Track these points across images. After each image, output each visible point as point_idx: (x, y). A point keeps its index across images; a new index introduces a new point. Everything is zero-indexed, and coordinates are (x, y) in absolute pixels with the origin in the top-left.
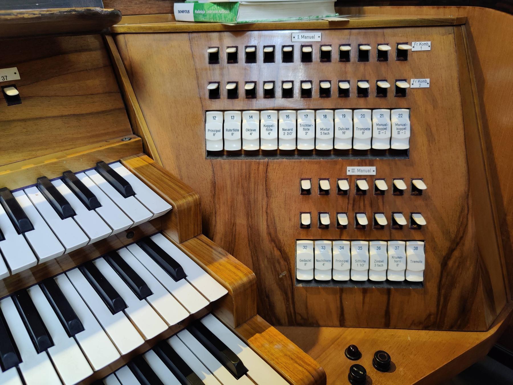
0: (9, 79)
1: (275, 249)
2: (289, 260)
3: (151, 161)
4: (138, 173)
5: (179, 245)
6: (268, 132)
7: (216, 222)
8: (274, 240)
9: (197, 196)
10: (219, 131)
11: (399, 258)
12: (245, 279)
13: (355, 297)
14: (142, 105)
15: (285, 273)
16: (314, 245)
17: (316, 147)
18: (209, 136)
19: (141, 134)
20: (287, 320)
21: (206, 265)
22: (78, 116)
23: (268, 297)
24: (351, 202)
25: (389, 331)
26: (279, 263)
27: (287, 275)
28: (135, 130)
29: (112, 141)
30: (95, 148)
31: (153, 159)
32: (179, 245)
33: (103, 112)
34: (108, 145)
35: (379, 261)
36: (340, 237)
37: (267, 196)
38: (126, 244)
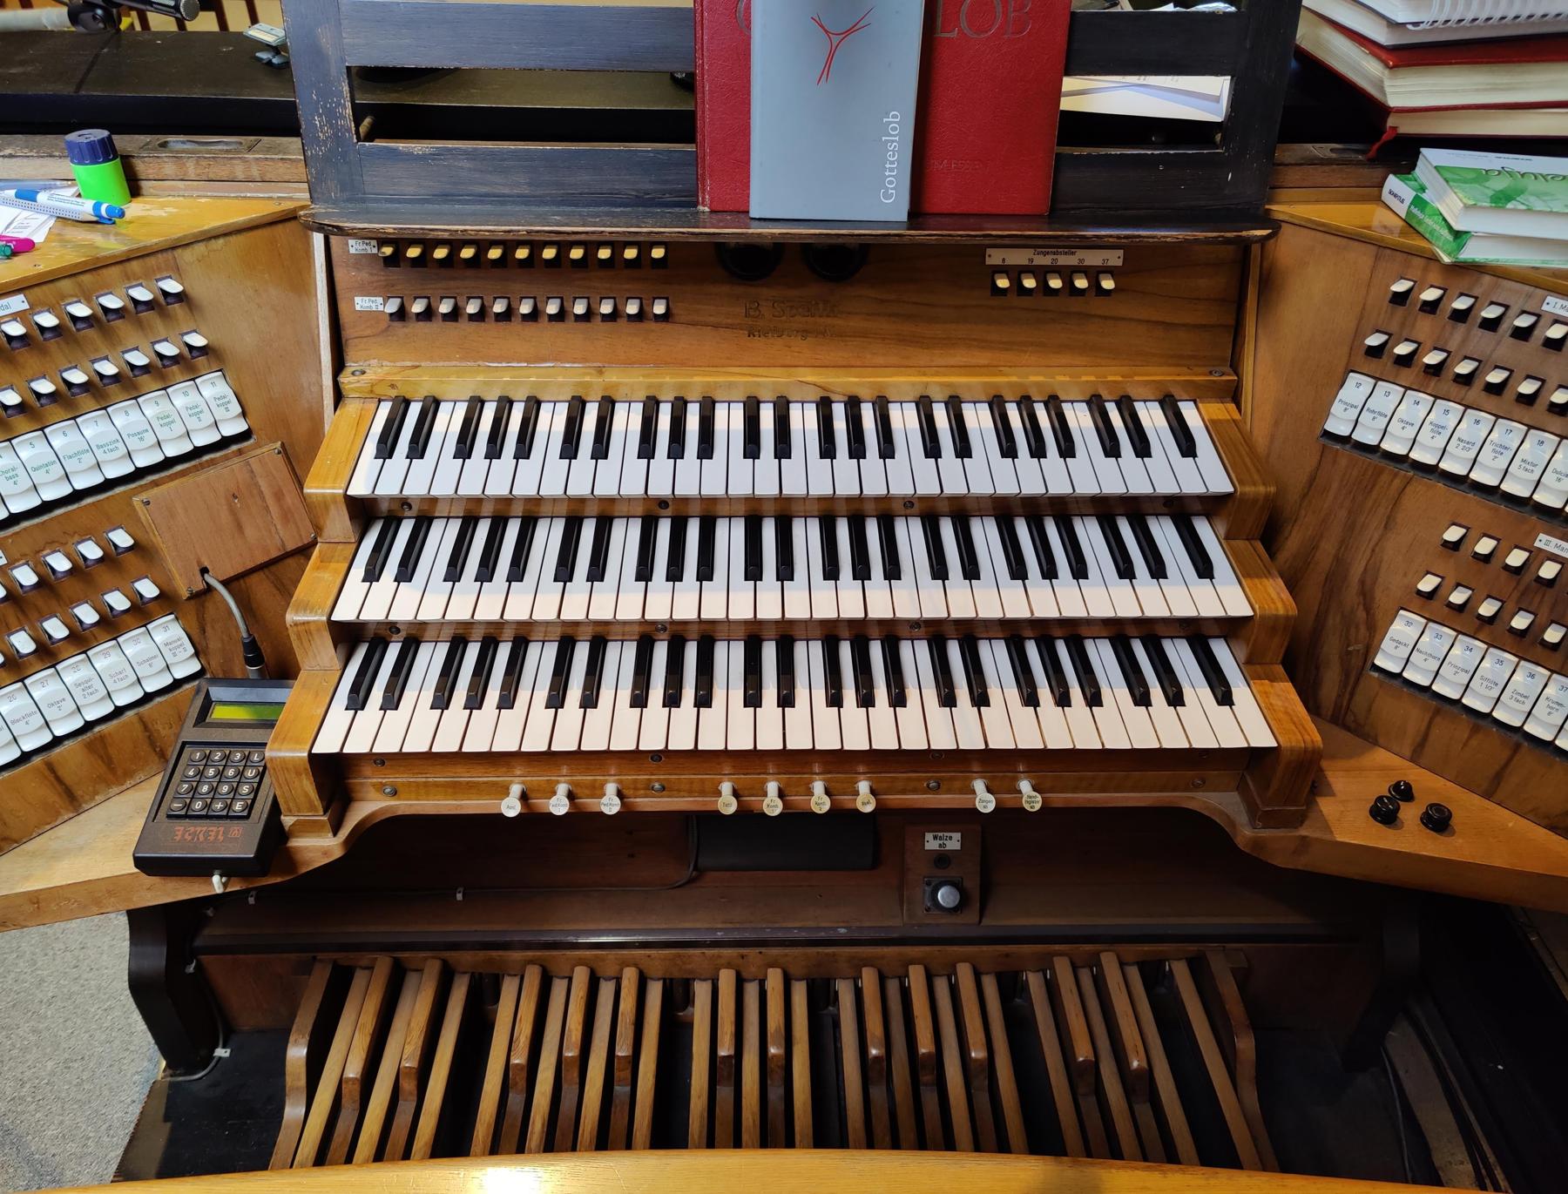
0: (1110, 263)
1: (1361, 607)
2: (1375, 631)
3: (1237, 416)
4: (1212, 427)
5: (1223, 542)
6: (1432, 435)
7: (1290, 534)
8: (1366, 595)
9: (1272, 489)
10: (1356, 407)
11: (1558, 703)
12: (1281, 612)
13: (1455, 729)
14: (1261, 335)
15: (1360, 647)
16: (1456, 638)
18: (1337, 408)
19: (1240, 372)
20: (1330, 713)
21: (1243, 576)
22: (1168, 326)
23: (1317, 668)
24: (1521, 588)
25: (1487, 803)
26: (1357, 627)
27: (1361, 652)
28: (1235, 365)
29: (1196, 369)
30: (1171, 375)
31: (1240, 411)
32: (1223, 542)
33: (1204, 326)
34: (1189, 375)
35: (1521, 695)
36: (1475, 633)
37: (1385, 527)
38: (1158, 512)
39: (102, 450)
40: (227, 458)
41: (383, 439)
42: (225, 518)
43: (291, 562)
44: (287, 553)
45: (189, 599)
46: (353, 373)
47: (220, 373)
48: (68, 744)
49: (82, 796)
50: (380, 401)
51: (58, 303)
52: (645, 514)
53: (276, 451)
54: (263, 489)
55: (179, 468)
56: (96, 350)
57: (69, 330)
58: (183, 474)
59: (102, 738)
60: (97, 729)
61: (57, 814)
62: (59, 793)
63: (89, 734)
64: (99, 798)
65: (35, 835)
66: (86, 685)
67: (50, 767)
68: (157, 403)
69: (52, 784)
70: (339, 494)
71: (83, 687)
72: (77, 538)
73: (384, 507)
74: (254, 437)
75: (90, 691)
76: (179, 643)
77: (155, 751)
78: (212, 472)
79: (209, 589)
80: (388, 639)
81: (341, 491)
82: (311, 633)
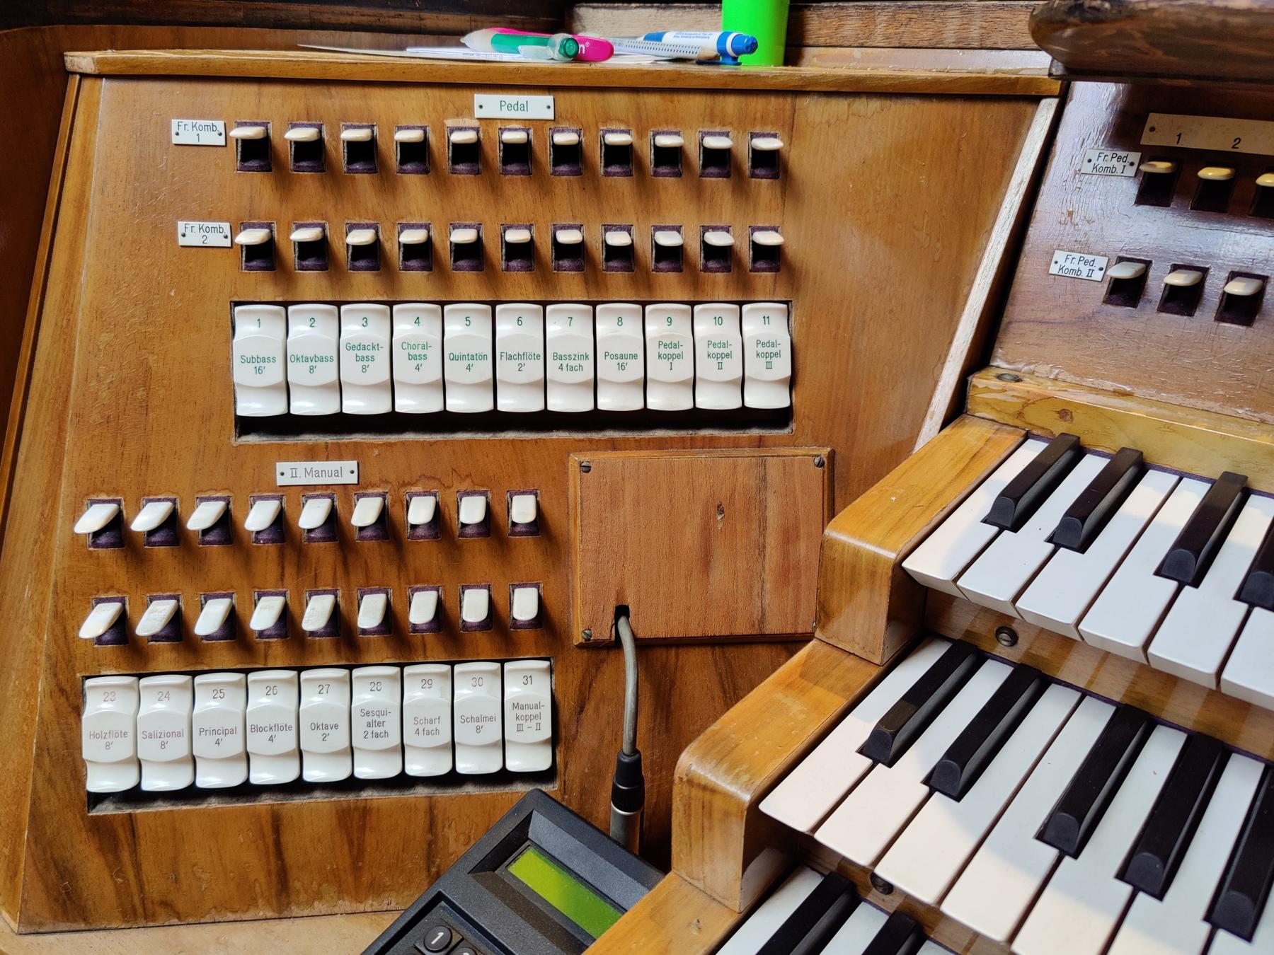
17: (746, 399)
39: (558, 362)
40: (736, 444)
41: (1012, 492)
42: (690, 537)
43: (763, 653)
44: (763, 635)
45: (581, 646)
46: (999, 377)
47: (784, 306)
48: (319, 797)
49: (298, 891)
50: (1027, 437)
51: (597, 126)
52: (1199, 729)
53: (817, 460)
54: (770, 513)
55: (659, 433)
56: (619, 212)
57: (593, 170)
58: (661, 444)
59: (365, 811)
60: (366, 794)
61: (252, 903)
62: (269, 871)
63: (351, 797)
64: (319, 907)
65: (207, 919)
66: (376, 718)
67: (277, 821)
68: (670, 320)
69: (267, 852)
70: (887, 560)
71: (370, 719)
72: (466, 485)
73: (960, 623)
74: (793, 426)
75: (378, 730)
76: (534, 712)
77: (429, 870)
78: (702, 458)
79: (617, 644)
80: (861, 892)
81: (892, 556)
82: (710, 814)
